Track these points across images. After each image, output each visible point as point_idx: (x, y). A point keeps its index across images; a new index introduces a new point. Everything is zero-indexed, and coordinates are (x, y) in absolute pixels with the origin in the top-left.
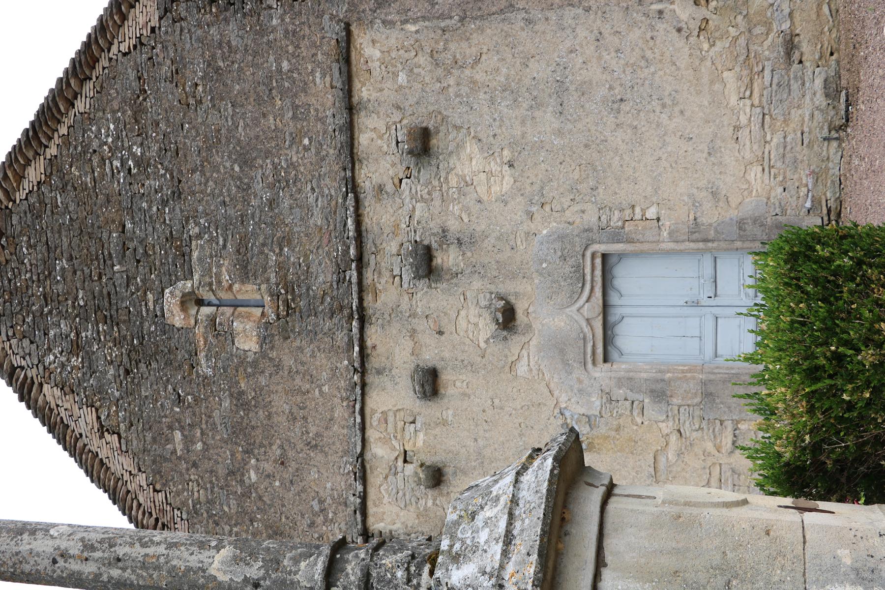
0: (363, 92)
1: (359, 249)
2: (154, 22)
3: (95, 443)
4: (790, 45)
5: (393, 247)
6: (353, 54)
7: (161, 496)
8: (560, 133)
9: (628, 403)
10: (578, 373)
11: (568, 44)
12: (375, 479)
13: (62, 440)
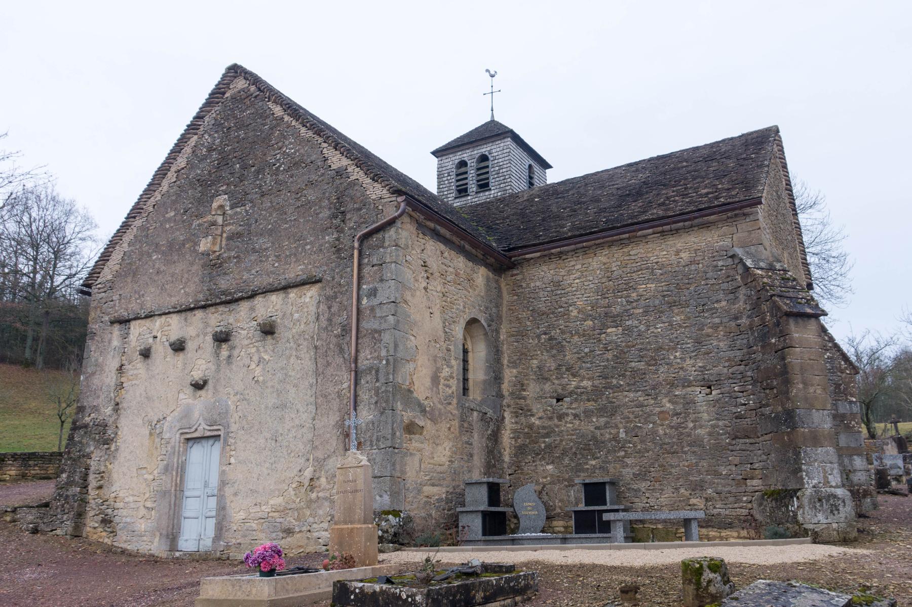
0: (293, 294)
1: (480, 143)
2: (333, 167)
3: (174, 168)
4: (289, 532)
5: (231, 321)
6: (308, 286)
7: (151, 209)
8: (267, 407)
9: (165, 453)
10: (178, 426)
11: (301, 409)
12: (147, 322)
13: (172, 152)
